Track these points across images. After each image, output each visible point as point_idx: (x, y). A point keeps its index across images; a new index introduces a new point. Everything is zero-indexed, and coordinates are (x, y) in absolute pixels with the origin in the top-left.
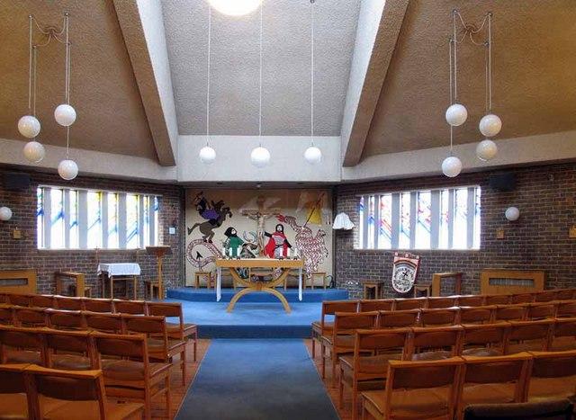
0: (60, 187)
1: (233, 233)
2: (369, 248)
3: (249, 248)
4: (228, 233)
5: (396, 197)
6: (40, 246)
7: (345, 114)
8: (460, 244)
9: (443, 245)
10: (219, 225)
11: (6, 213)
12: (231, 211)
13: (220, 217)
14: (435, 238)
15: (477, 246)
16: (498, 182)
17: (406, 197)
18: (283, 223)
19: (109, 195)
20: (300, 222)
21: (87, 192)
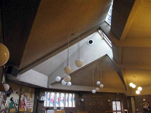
0: (55, 92)
1: (13, 99)
2: (47, 106)
3: (16, 105)
4: (11, 99)
5: (65, 94)
6: (45, 106)
7: (134, 100)
8: (70, 106)
9: (67, 106)
10: (9, 96)
11: (117, 106)
12: (13, 91)
13: (10, 93)
14: (65, 105)
15: (74, 106)
16: (79, 94)
17: (58, 94)
18: (25, 97)
19: (57, 93)
20: (28, 97)
21: (56, 93)
